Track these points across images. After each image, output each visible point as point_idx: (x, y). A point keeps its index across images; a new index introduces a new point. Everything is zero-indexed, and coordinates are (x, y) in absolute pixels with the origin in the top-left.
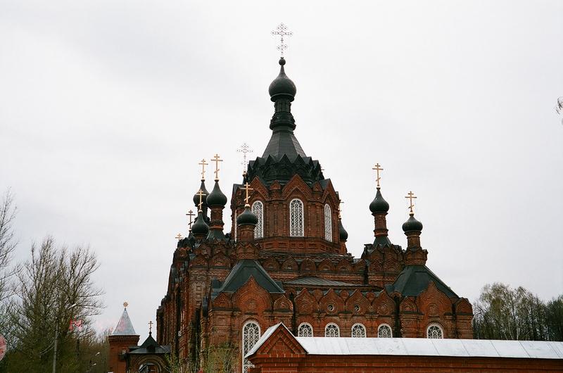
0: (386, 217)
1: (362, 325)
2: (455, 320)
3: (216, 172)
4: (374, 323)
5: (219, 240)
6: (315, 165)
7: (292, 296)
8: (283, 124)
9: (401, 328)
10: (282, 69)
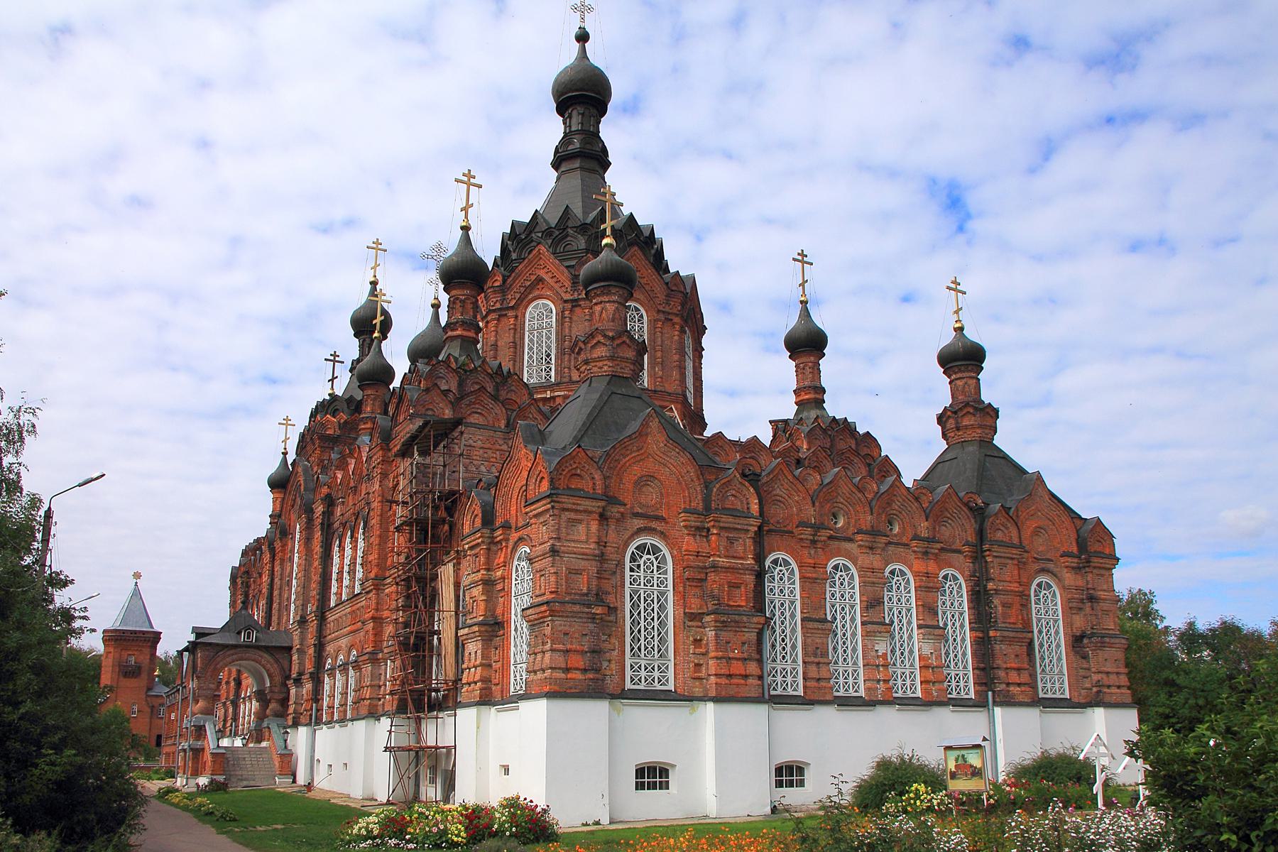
9: (988, 580)
10: (583, 51)
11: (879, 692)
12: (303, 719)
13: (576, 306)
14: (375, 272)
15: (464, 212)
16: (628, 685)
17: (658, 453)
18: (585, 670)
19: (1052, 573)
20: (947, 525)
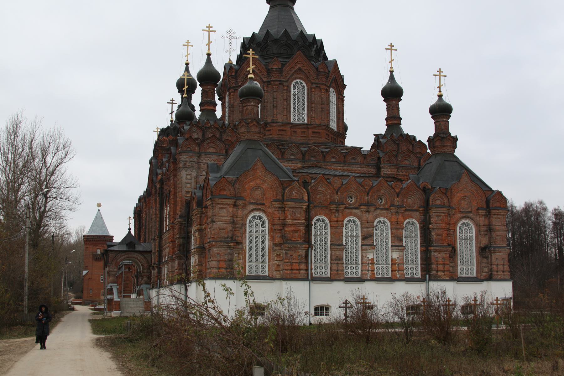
0: (400, 103)
1: (386, 220)
2: (488, 214)
3: (208, 44)
5: (212, 123)
7: (305, 184)
9: (430, 223)
11: (368, 275)
12: (155, 286)
13: (269, 84)
14: (187, 58)
15: (210, 41)
16: (247, 273)
17: (262, 176)
19: (470, 218)
20: (412, 198)
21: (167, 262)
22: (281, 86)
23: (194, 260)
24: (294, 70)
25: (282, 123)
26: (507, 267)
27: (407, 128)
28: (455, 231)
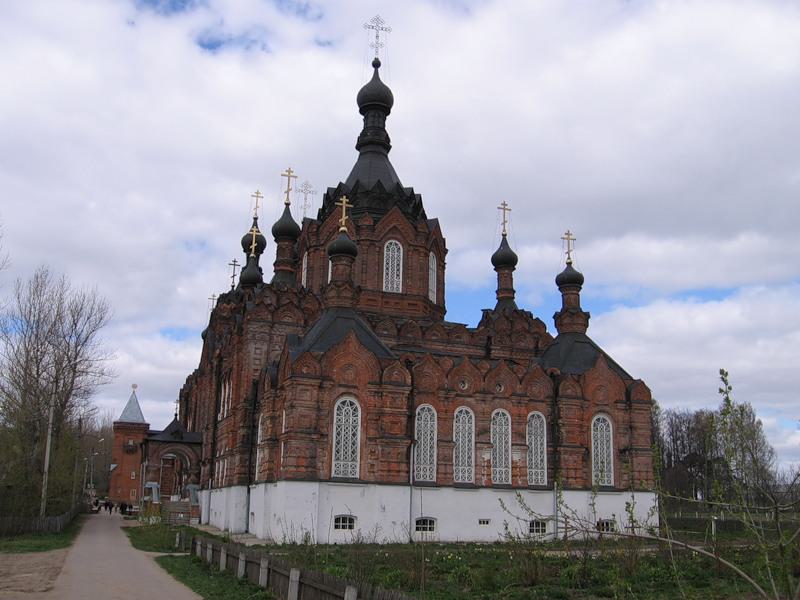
4: (523, 410)
6: (418, 199)
7: (408, 364)
8: (374, 142)
9: (560, 418)
10: (376, 73)
16: (333, 474)
18: (307, 467)
21: (223, 457)
22: (372, 247)
23: (260, 455)
24: (388, 228)
25: (373, 291)
26: (651, 475)
27: (522, 301)
28: (589, 428)
